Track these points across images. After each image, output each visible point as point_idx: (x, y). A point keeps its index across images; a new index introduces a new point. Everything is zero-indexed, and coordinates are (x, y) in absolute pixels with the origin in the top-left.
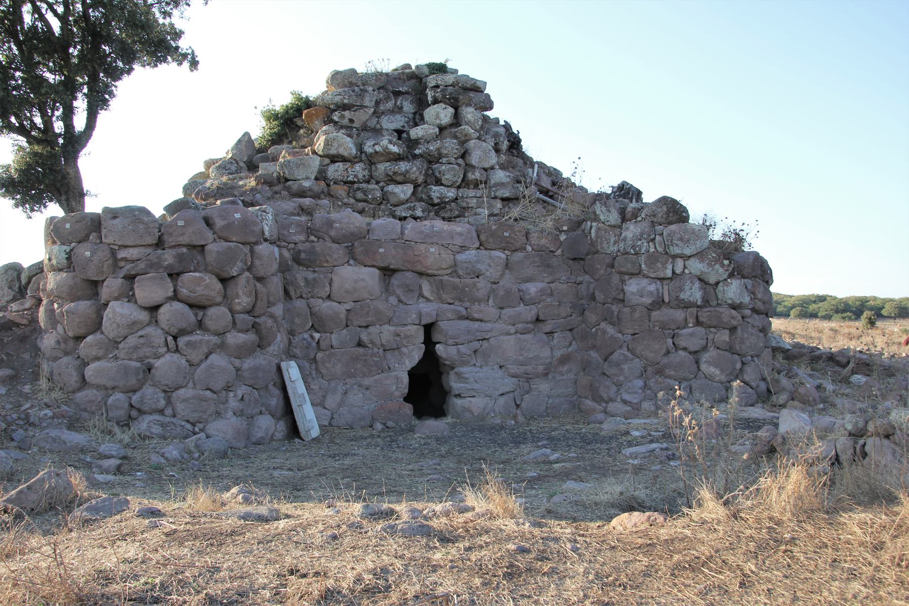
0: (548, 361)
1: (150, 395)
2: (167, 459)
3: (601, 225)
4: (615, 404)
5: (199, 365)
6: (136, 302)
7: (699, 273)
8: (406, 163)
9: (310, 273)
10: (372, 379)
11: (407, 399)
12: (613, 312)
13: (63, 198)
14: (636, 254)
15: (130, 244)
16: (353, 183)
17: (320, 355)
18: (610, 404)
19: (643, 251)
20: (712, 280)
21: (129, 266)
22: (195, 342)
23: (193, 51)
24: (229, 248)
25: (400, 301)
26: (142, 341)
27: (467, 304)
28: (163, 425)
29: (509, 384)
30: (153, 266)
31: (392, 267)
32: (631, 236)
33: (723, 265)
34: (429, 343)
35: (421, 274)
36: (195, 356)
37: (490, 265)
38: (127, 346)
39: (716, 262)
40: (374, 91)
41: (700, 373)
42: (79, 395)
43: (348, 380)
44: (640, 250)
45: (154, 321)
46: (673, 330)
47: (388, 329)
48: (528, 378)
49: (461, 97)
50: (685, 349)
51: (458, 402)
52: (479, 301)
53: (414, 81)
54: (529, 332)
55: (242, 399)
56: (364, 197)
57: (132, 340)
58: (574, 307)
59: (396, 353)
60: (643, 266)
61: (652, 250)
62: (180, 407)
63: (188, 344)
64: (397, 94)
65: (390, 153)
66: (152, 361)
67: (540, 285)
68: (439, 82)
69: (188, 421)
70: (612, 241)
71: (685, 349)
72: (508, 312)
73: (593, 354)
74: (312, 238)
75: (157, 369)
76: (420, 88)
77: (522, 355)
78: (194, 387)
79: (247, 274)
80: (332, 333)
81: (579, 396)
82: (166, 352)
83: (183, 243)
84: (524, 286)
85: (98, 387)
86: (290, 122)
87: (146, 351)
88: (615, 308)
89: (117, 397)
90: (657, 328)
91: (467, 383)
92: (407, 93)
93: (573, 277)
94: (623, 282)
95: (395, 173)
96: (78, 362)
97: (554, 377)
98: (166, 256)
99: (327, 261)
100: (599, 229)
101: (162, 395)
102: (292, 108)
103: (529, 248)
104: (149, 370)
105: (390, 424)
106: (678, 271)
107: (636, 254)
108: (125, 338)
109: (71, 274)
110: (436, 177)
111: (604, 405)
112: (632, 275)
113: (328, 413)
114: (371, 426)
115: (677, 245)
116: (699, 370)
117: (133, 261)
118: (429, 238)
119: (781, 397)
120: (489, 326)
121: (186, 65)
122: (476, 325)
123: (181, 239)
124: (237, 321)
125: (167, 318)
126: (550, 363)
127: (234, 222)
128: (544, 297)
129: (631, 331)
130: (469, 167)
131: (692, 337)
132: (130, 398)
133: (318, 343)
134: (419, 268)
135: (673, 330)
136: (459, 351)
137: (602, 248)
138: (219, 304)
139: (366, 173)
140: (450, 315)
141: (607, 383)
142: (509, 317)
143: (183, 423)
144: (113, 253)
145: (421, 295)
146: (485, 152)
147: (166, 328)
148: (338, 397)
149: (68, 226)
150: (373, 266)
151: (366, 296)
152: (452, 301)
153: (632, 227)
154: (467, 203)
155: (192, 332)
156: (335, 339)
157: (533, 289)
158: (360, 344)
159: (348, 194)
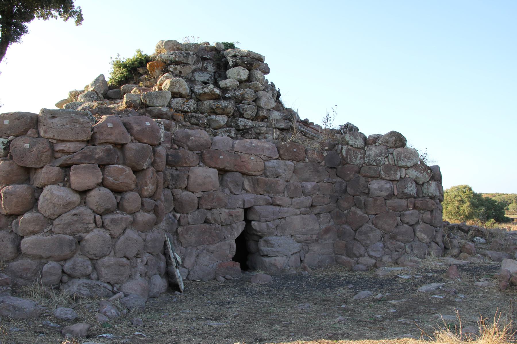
0: (318, 232)
1: (80, 262)
2: (108, 317)
3: (349, 147)
4: (365, 258)
5: (118, 238)
6: (70, 187)
7: (415, 177)
9: (174, 171)
10: (215, 246)
11: (235, 259)
12: (361, 201)
14: (377, 165)
15: (68, 139)
16: (187, 112)
17: (180, 229)
18: (361, 258)
19: (382, 163)
20: (421, 182)
21: (64, 157)
22: (118, 220)
23: (81, 10)
24: (143, 147)
25: (231, 192)
26: (75, 218)
27: (272, 195)
28: (90, 287)
29: (296, 247)
31: (227, 168)
32: (374, 154)
33: (428, 173)
34: (248, 221)
35: (243, 174)
36: (116, 230)
37: (285, 170)
38: (62, 222)
39: (424, 171)
40: (194, 55)
41: (416, 238)
42: (14, 264)
43: (198, 247)
44: (380, 163)
45: (84, 203)
46: (400, 212)
47: (224, 212)
49: (254, 64)
50: (407, 223)
51: (267, 260)
52: (279, 193)
53: (214, 52)
54: (308, 214)
55: (146, 264)
56: (196, 121)
57: (66, 218)
58: (331, 197)
59: (229, 227)
60: (382, 172)
61: (387, 163)
62: (104, 271)
63: (113, 221)
64: (204, 59)
65: (215, 94)
66: (83, 235)
67: (314, 184)
68: (237, 54)
69: (109, 283)
70: (359, 157)
71: (407, 223)
72: (296, 200)
73: (347, 227)
74: (175, 146)
75: (87, 241)
76: (218, 59)
77: (304, 228)
78: (115, 256)
79: (152, 168)
80: (188, 213)
81: (336, 254)
82: (94, 228)
83: (111, 141)
84: (305, 184)
85: (33, 257)
86: (135, 70)
87: (79, 226)
88: (362, 198)
89: (52, 265)
90: (391, 211)
91: (273, 247)
92: (210, 59)
93: (330, 179)
94: (367, 182)
95: (217, 107)
96: (12, 236)
97: (322, 242)
98: (98, 150)
99: (186, 163)
100: (348, 150)
101: (89, 262)
102: (136, 61)
103: (307, 160)
104: (79, 242)
105: (228, 277)
106: (403, 176)
107: (377, 165)
108: (60, 215)
109: (8, 162)
110: (240, 112)
111: (356, 259)
112: (374, 178)
113: (186, 271)
114: (215, 279)
115: (403, 160)
116: (415, 236)
117: (69, 153)
118: (250, 151)
119: (454, 251)
120: (285, 209)
121: (72, 20)
122: (278, 208)
123: (109, 137)
124: (145, 203)
125: (97, 200)
126: (319, 234)
127: (146, 128)
128: (315, 191)
129: (374, 213)
130: (259, 108)
131: (411, 215)
132: (62, 266)
133: (179, 221)
134: (244, 170)
135: (400, 212)
136: (268, 226)
137: (351, 161)
138: (132, 190)
139: (195, 106)
140: (261, 202)
141: (358, 245)
142: (297, 204)
143: (106, 285)
144: (52, 146)
145: (243, 189)
146: (268, 100)
147: (95, 208)
148: (193, 259)
149: (6, 122)
150: (215, 168)
151: (211, 188)
152: (263, 193)
153: (374, 149)
154: (260, 130)
155: (113, 212)
156: (190, 218)
157: (309, 185)
158: (207, 221)
159: (185, 119)
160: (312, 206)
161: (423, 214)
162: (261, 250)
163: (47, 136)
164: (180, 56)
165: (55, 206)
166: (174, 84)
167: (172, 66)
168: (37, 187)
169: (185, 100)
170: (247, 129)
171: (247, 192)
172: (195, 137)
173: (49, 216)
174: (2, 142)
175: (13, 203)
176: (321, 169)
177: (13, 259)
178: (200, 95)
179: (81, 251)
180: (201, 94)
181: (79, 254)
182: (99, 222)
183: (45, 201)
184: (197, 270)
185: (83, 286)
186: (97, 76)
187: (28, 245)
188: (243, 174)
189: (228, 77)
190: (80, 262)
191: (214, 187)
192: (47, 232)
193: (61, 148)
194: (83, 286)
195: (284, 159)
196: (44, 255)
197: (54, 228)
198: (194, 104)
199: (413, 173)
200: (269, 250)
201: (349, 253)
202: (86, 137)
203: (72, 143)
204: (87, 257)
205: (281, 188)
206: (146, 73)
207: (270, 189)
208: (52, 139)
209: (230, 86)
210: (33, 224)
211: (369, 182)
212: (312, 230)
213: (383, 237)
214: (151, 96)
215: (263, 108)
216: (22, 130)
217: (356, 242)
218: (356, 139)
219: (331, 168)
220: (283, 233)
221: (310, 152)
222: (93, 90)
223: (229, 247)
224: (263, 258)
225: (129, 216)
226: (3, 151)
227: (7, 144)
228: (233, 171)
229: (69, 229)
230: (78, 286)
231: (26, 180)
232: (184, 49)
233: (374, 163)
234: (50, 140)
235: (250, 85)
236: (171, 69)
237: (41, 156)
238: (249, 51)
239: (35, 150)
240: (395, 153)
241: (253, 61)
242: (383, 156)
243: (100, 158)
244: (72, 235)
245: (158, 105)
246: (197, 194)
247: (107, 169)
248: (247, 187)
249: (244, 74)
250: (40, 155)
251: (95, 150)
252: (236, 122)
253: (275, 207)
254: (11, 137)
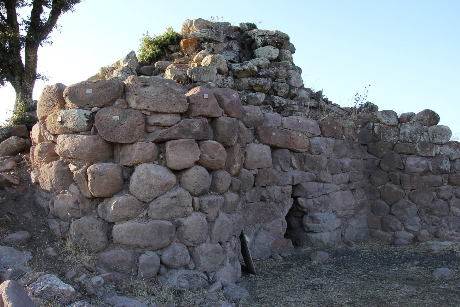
0: (354, 207)
3: (382, 125)
8: (264, 79)
10: (271, 224)
12: (396, 177)
13: (17, 78)
15: (164, 110)
19: (418, 140)
20: (453, 159)
26: (174, 201)
30: (185, 132)
31: (278, 145)
32: (409, 131)
34: (295, 198)
35: (291, 151)
38: (160, 206)
43: (256, 226)
44: (416, 140)
46: (435, 187)
47: (277, 189)
48: (347, 218)
50: (442, 198)
51: (313, 236)
53: (238, 32)
57: (164, 201)
58: (364, 173)
60: (418, 149)
61: (422, 140)
62: (202, 259)
63: (210, 203)
66: (181, 220)
68: (265, 33)
69: (205, 272)
70: (393, 135)
71: (442, 198)
75: (185, 227)
76: (244, 40)
77: (344, 204)
83: (206, 114)
84: (343, 160)
85: (128, 247)
86: (166, 47)
87: (178, 210)
88: (398, 174)
90: (427, 186)
91: (318, 223)
95: (257, 85)
98: (195, 124)
102: (168, 38)
103: (344, 137)
105: (286, 255)
106: (438, 153)
107: (413, 142)
108: (156, 198)
110: (274, 90)
111: (393, 233)
112: (409, 154)
114: (271, 257)
115: (439, 138)
117: (164, 127)
120: (328, 186)
122: (322, 185)
125: (195, 179)
127: (234, 101)
128: (351, 167)
129: (410, 188)
130: (291, 87)
134: (293, 147)
135: (435, 187)
136: (314, 202)
137: (384, 138)
140: (307, 179)
143: (203, 274)
145: (292, 166)
147: (192, 189)
151: (265, 165)
153: (409, 127)
154: (293, 108)
158: (263, 199)
160: (349, 182)
161: (456, 189)
162: (307, 226)
163: (140, 106)
164: (212, 34)
165: (151, 188)
166: (215, 60)
167: (206, 43)
168: (126, 166)
169: (224, 76)
170: (282, 106)
171: (294, 168)
172: (250, 113)
173: (144, 199)
174: (85, 114)
175: (103, 184)
176: (355, 146)
177: (103, 250)
178: (238, 72)
179: (178, 238)
180: (240, 71)
181: (176, 242)
182: (197, 206)
183: (140, 182)
184: (256, 249)
185: (183, 278)
186: (128, 53)
187: (123, 233)
188: (291, 151)
189: (257, 55)
190: (178, 251)
191: (268, 164)
192: (142, 218)
193: (157, 121)
194: (183, 278)
195: (325, 136)
196: (142, 245)
197: (151, 212)
198: (232, 81)
199: (447, 150)
200: (315, 226)
201: (384, 227)
202: (182, 109)
203: (167, 115)
204: (185, 244)
205: (324, 164)
206: (178, 50)
207: (315, 166)
208: (145, 110)
209: (263, 64)
210: (127, 208)
211: (404, 158)
212: (350, 205)
213: (419, 212)
214: (198, 71)
215: (294, 87)
216: (109, 100)
217: (392, 216)
218: (390, 117)
219: (363, 145)
220: (326, 209)
221: (347, 129)
222: (127, 66)
223: (280, 225)
224: (308, 234)
225: (220, 197)
226: (86, 124)
227: (90, 116)
228: (283, 148)
229: (167, 214)
230: (178, 278)
231: (110, 157)
232: (214, 28)
233: (410, 141)
234: (143, 112)
235: (280, 64)
236: (205, 46)
237: (134, 130)
238: (277, 31)
239: (126, 122)
240: (430, 130)
241: (283, 41)
242: (419, 133)
243: (197, 133)
244: (170, 221)
245: (205, 80)
246: (253, 171)
247: (203, 145)
248: (294, 164)
249: (275, 53)
250: (132, 129)
251: (192, 124)
252: (271, 99)
253: (319, 183)
254: (96, 108)
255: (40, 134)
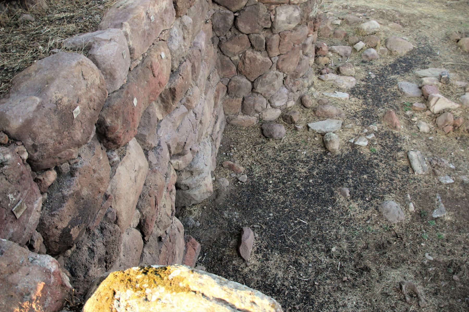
88: (263, 36)
255: (41, 220)
